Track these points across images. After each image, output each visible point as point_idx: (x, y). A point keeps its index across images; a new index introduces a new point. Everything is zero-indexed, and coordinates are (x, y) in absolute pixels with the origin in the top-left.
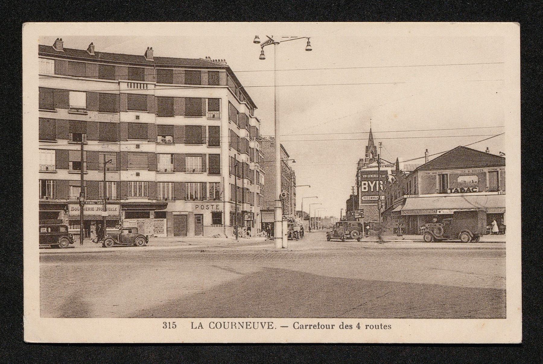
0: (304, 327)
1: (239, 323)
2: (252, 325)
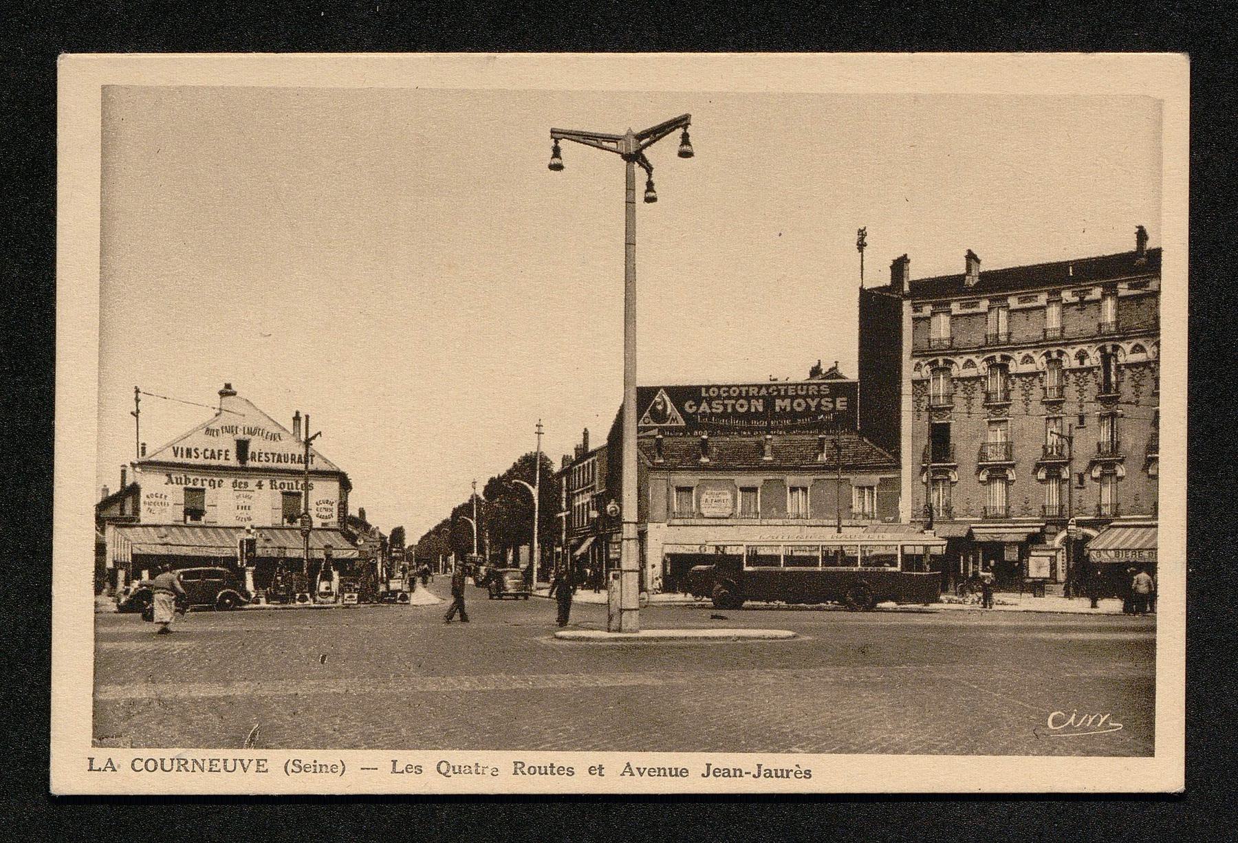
2: (220, 765)
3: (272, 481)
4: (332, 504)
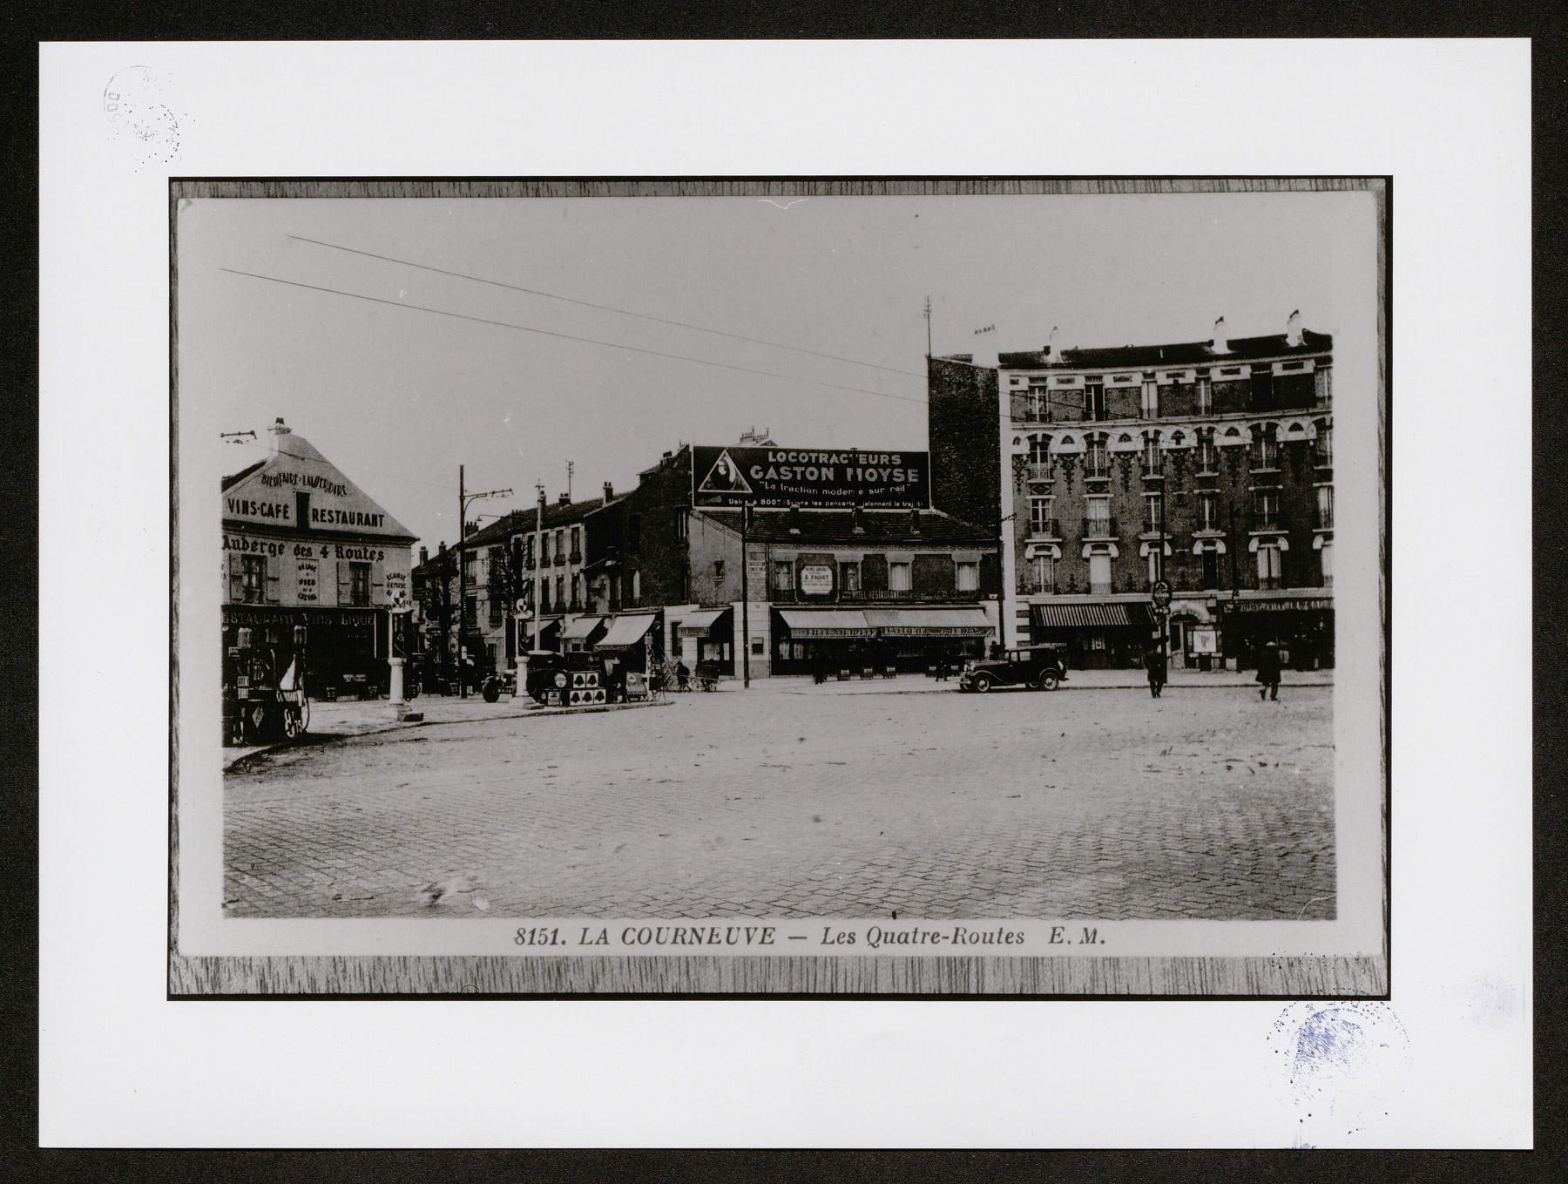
1: (694, 930)
3: (337, 547)
4: (403, 578)
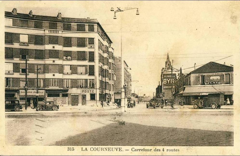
0: (137, 150)
1: (105, 148)
2: (111, 149)
